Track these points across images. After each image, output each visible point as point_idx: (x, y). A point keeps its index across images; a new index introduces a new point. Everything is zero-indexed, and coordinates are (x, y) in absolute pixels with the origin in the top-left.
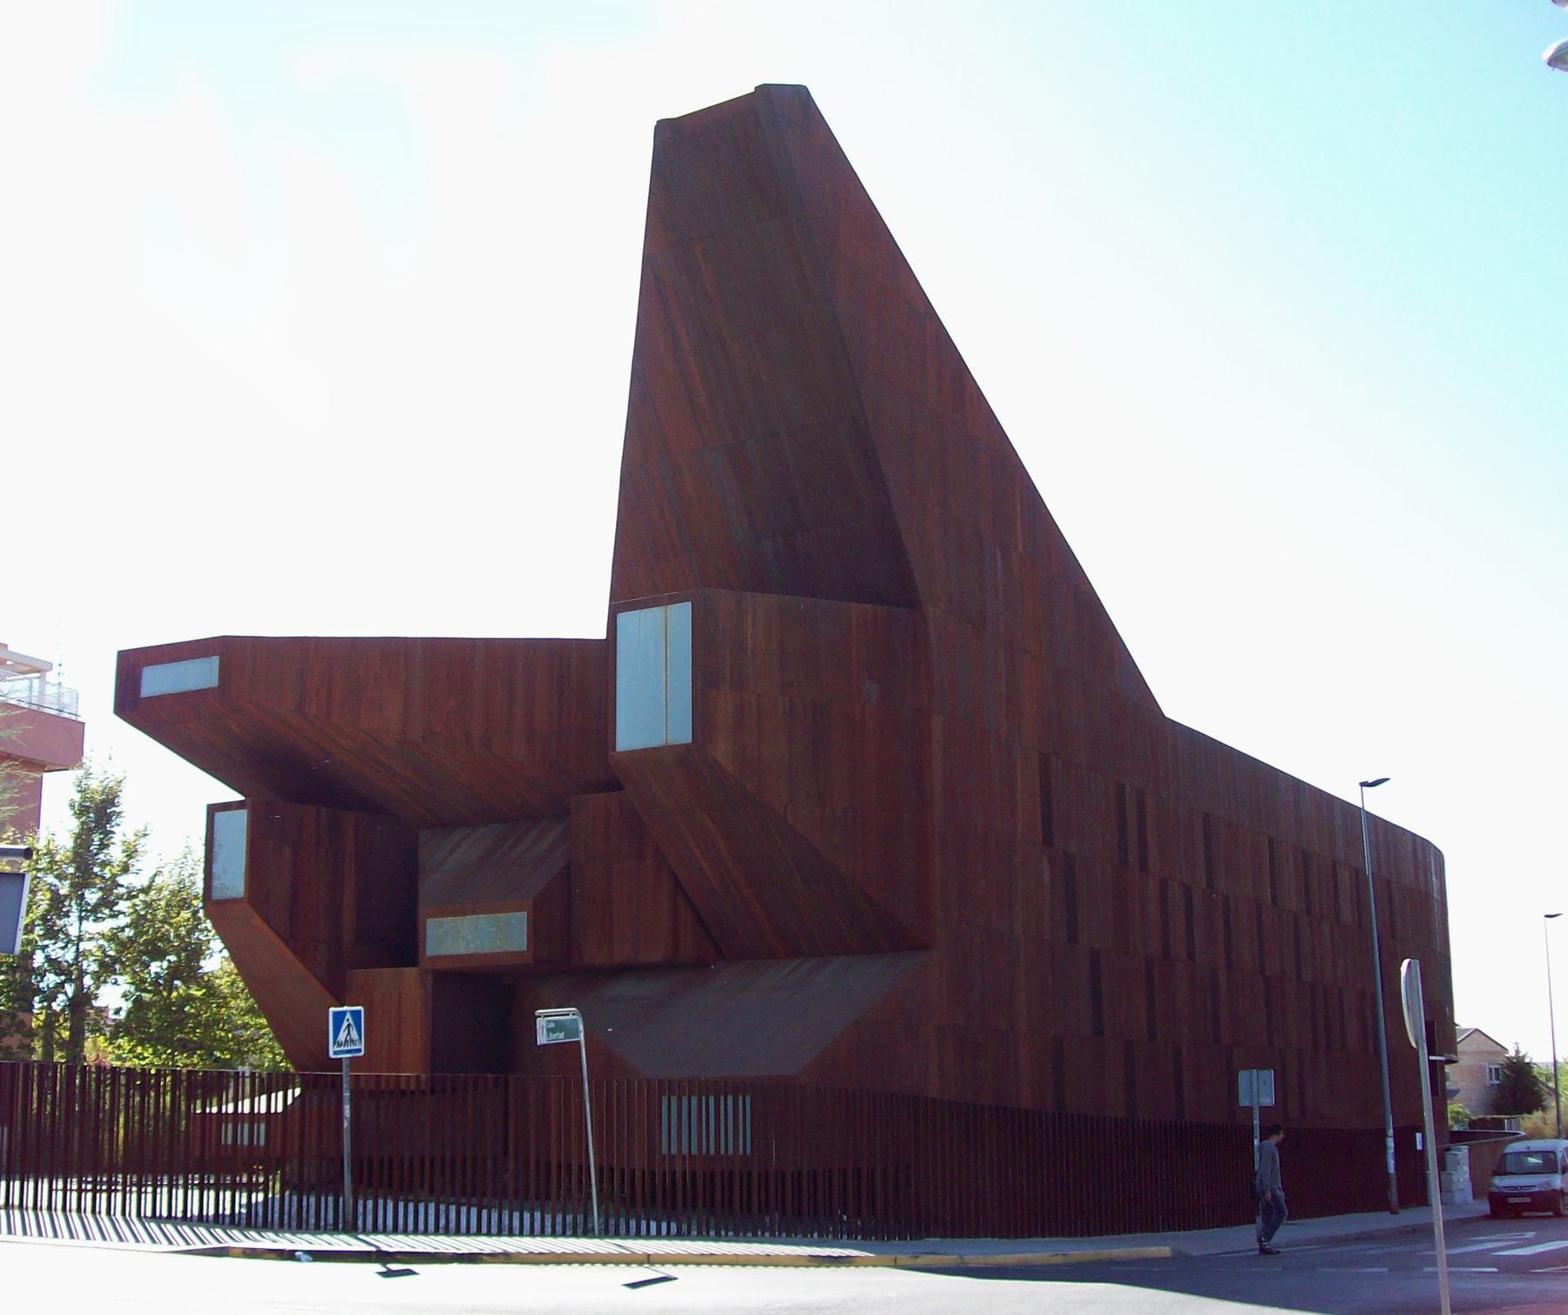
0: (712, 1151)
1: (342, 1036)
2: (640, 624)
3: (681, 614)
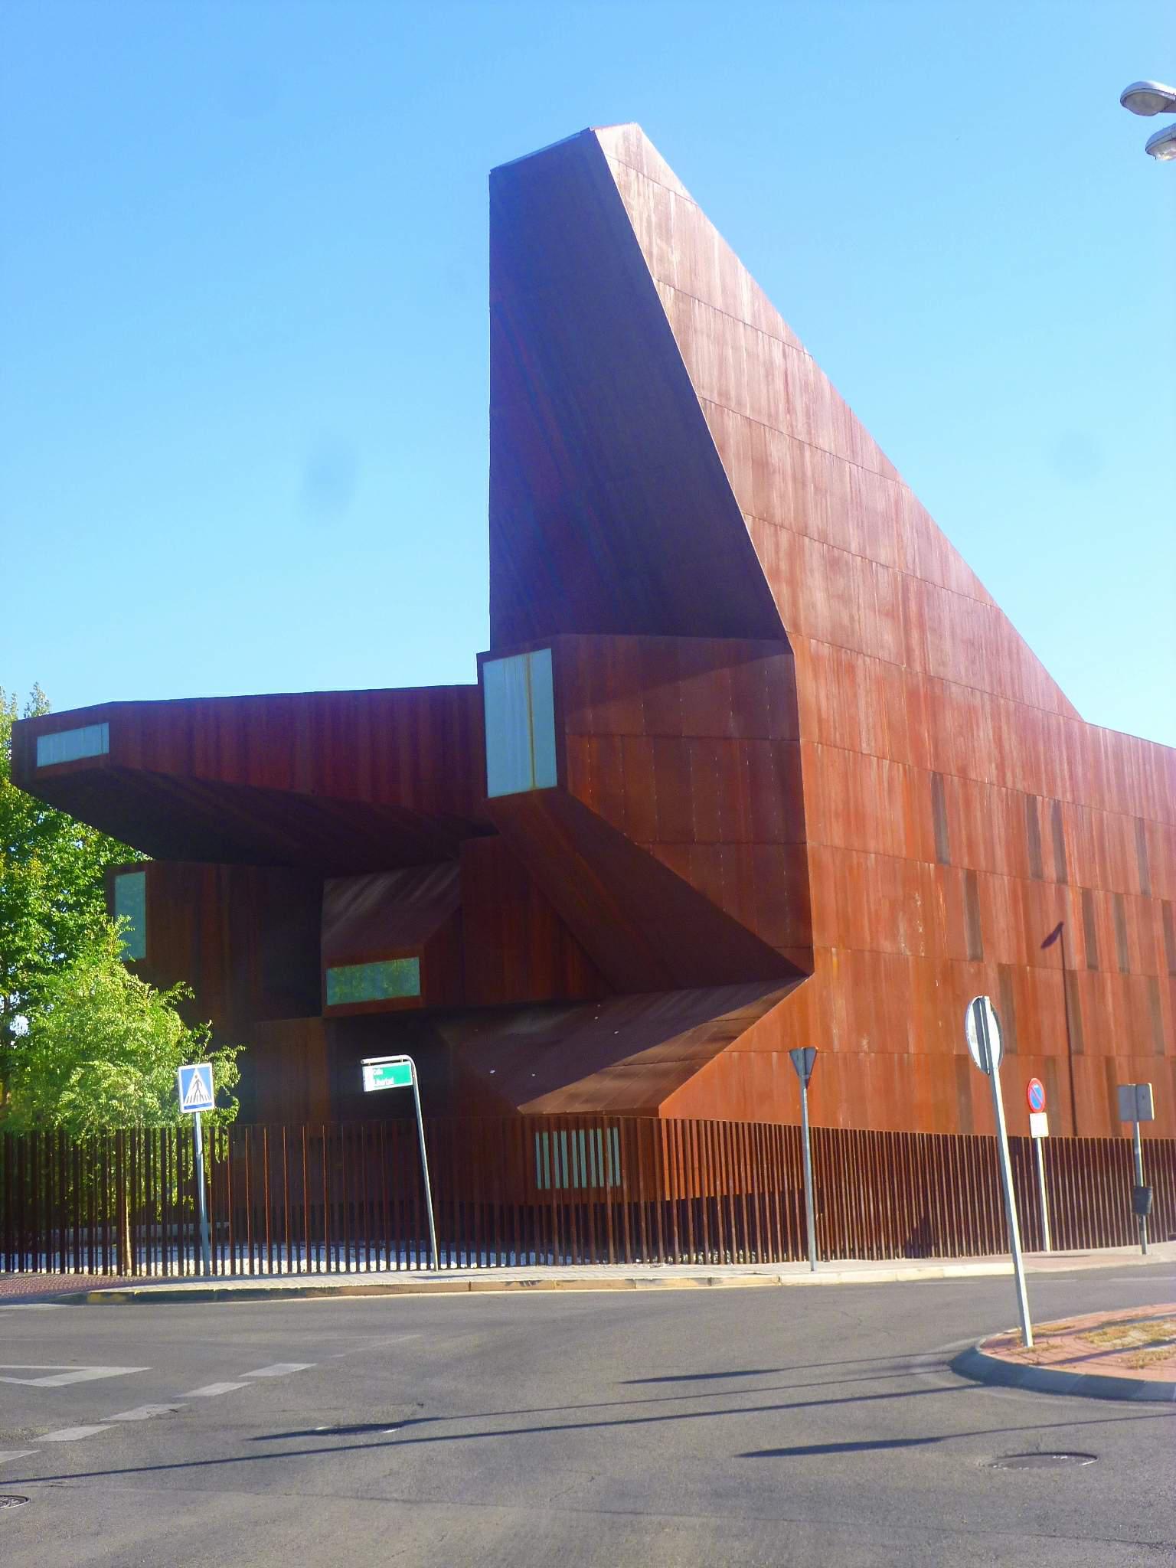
1: (191, 1092)
2: (509, 671)
3: (542, 661)
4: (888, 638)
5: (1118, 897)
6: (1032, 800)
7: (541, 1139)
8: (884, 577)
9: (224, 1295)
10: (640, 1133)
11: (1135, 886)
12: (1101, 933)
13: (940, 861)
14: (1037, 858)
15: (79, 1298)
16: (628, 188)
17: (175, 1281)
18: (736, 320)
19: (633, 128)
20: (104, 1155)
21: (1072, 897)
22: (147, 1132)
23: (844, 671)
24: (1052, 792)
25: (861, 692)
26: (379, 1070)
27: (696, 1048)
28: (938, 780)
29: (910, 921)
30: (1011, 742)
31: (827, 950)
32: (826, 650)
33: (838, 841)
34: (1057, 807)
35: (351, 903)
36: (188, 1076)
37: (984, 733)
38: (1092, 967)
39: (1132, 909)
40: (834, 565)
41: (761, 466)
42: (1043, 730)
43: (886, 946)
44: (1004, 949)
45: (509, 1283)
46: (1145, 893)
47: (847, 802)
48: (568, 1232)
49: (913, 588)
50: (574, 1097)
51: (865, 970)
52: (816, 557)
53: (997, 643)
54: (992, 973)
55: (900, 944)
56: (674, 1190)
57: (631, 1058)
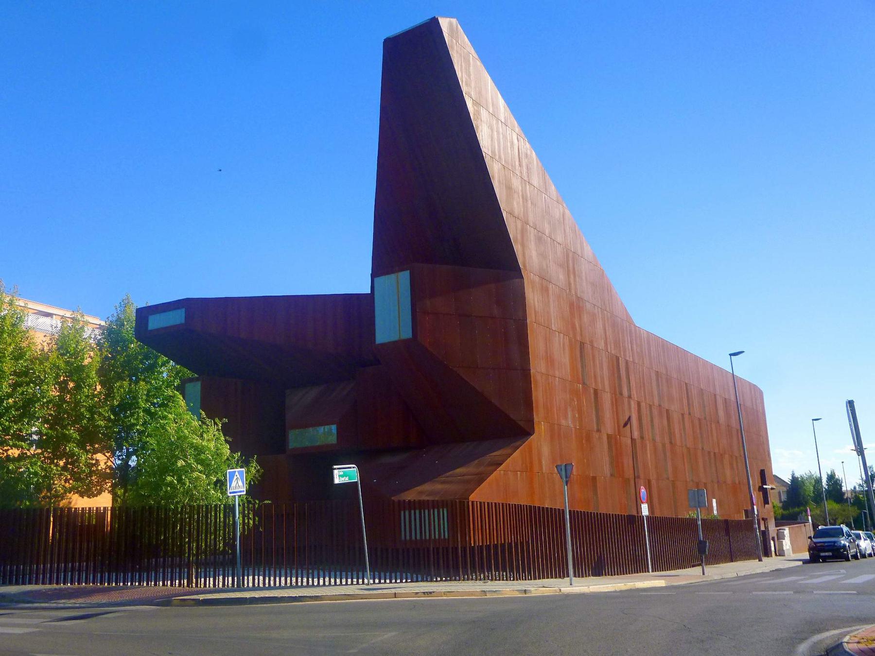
0: (437, 537)
1: (234, 484)
2: (386, 281)
3: (404, 277)
4: (561, 277)
5: (650, 406)
6: (618, 359)
7: (415, 514)
8: (559, 249)
9: (253, 600)
10: (458, 511)
11: (656, 402)
12: (644, 422)
13: (584, 384)
14: (620, 386)
15: (166, 601)
16: (452, 48)
17: (210, 592)
18: (498, 119)
19: (454, 21)
20: (182, 519)
21: (633, 405)
22: (207, 506)
23: (545, 290)
24: (625, 355)
25: (551, 300)
26: (341, 472)
27: (481, 469)
28: (582, 345)
29: (573, 411)
30: (609, 332)
31: (539, 422)
32: (537, 279)
33: (543, 370)
34: (627, 362)
35: (299, 400)
36: (232, 475)
37: (599, 325)
38: (642, 438)
39: (655, 412)
40: (539, 240)
41: (509, 188)
42: (621, 327)
43: (563, 422)
44: (609, 427)
45: (417, 593)
46: (660, 406)
47: (547, 353)
48: (438, 565)
49: (571, 255)
50: (421, 493)
51: (555, 433)
52: (532, 235)
53: (602, 287)
54: (605, 438)
55: (568, 422)
56: (476, 540)
57: (448, 474)
